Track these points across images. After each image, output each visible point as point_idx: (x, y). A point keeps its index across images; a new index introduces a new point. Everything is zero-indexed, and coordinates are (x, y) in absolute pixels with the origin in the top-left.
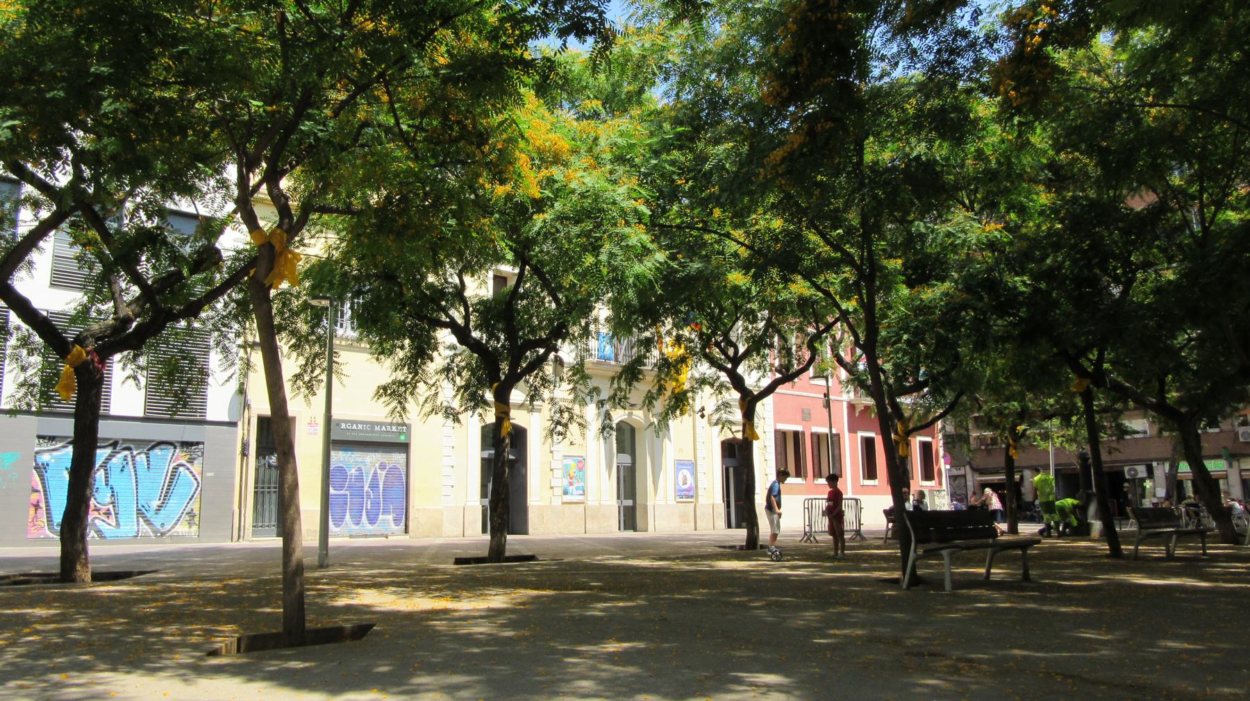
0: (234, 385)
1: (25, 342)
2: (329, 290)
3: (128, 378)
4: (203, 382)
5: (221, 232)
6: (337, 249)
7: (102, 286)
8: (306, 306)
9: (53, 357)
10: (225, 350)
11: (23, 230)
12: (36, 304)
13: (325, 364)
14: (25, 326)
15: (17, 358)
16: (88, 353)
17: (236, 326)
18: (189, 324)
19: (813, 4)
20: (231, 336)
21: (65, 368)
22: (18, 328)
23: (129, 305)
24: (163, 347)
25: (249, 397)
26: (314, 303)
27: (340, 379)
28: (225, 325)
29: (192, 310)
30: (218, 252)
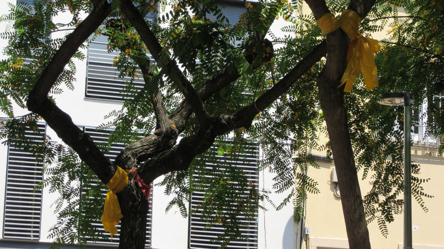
0: (289, 210)
1: (67, 165)
2: (401, 85)
3: (173, 203)
4: (254, 208)
5: (271, 18)
6: (409, 30)
7: (144, 99)
8: (374, 108)
9: (96, 181)
10: (281, 167)
11: (58, 36)
12: (77, 121)
13: (402, 179)
14: (66, 147)
15: (57, 183)
16: (130, 176)
17: (292, 135)
18: (238, 135)
19: (19, 2)
20: (287, 148)
21: (108, 195)
22: (60, 149)
23: (172, 116)
24: (209, 166)
25: (307, 225)
26: (386, 102)
27: (420, 201)
28: (280, 135)
29: (243, 120)
30: (269, 44)
